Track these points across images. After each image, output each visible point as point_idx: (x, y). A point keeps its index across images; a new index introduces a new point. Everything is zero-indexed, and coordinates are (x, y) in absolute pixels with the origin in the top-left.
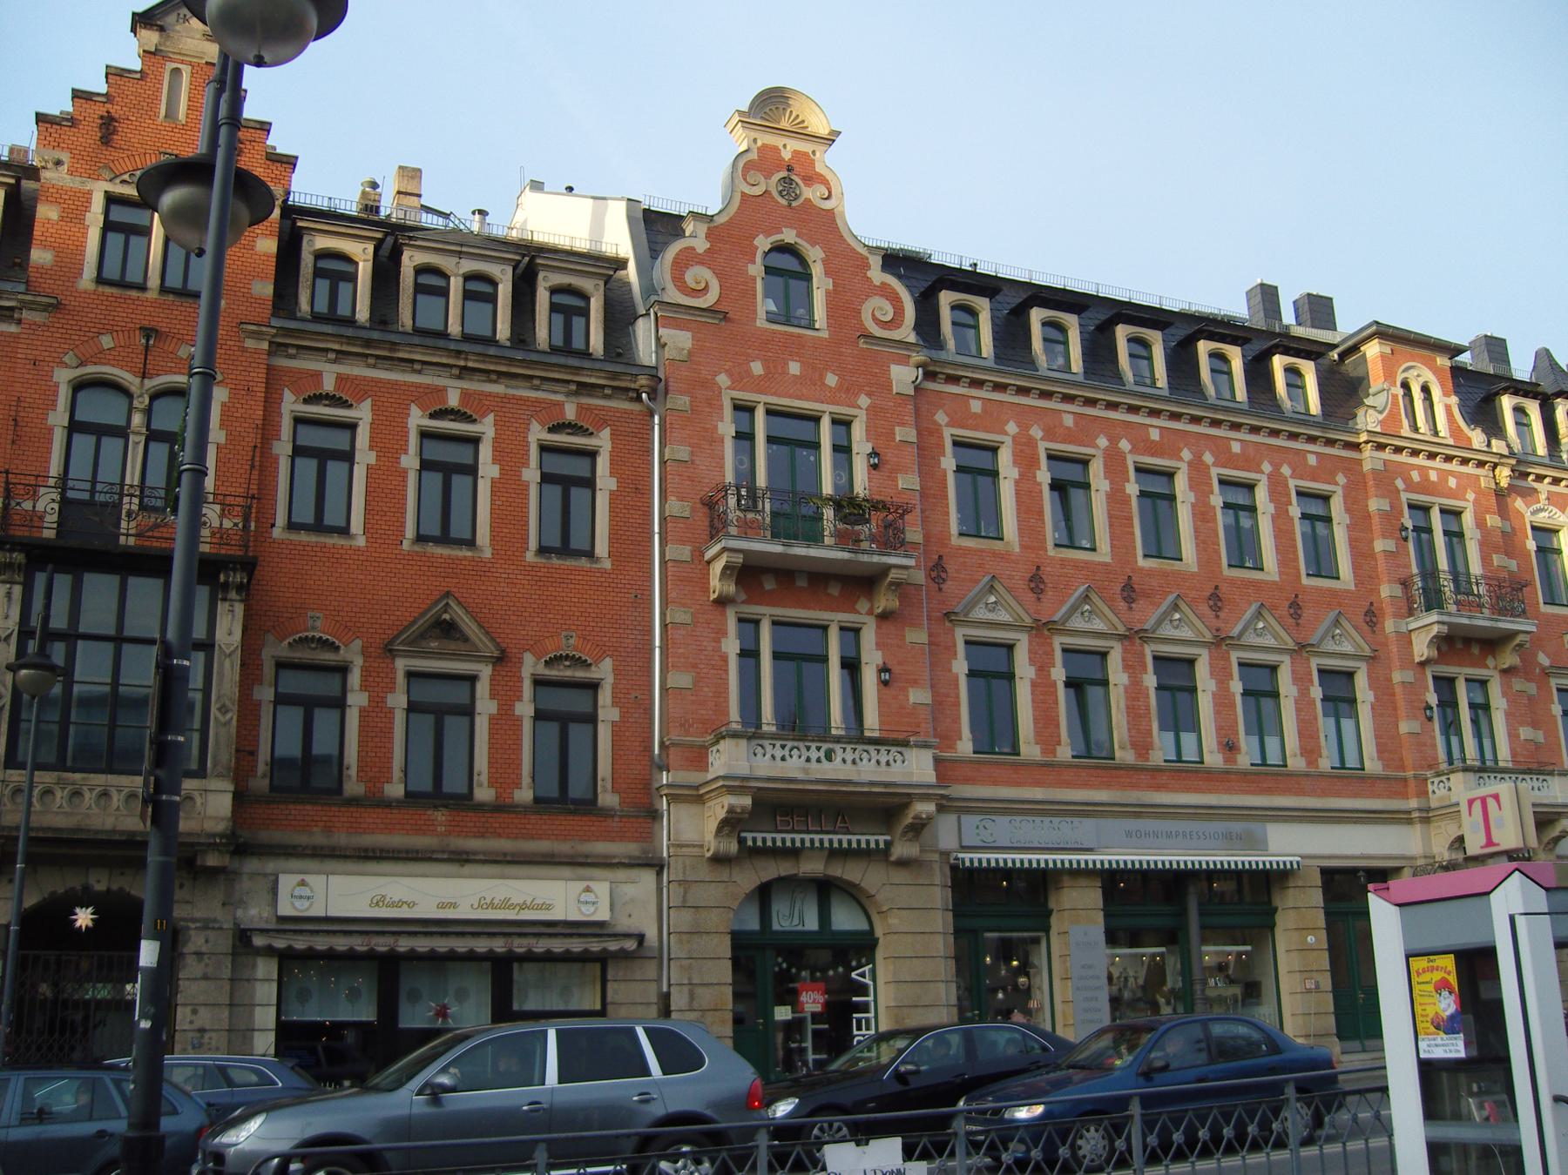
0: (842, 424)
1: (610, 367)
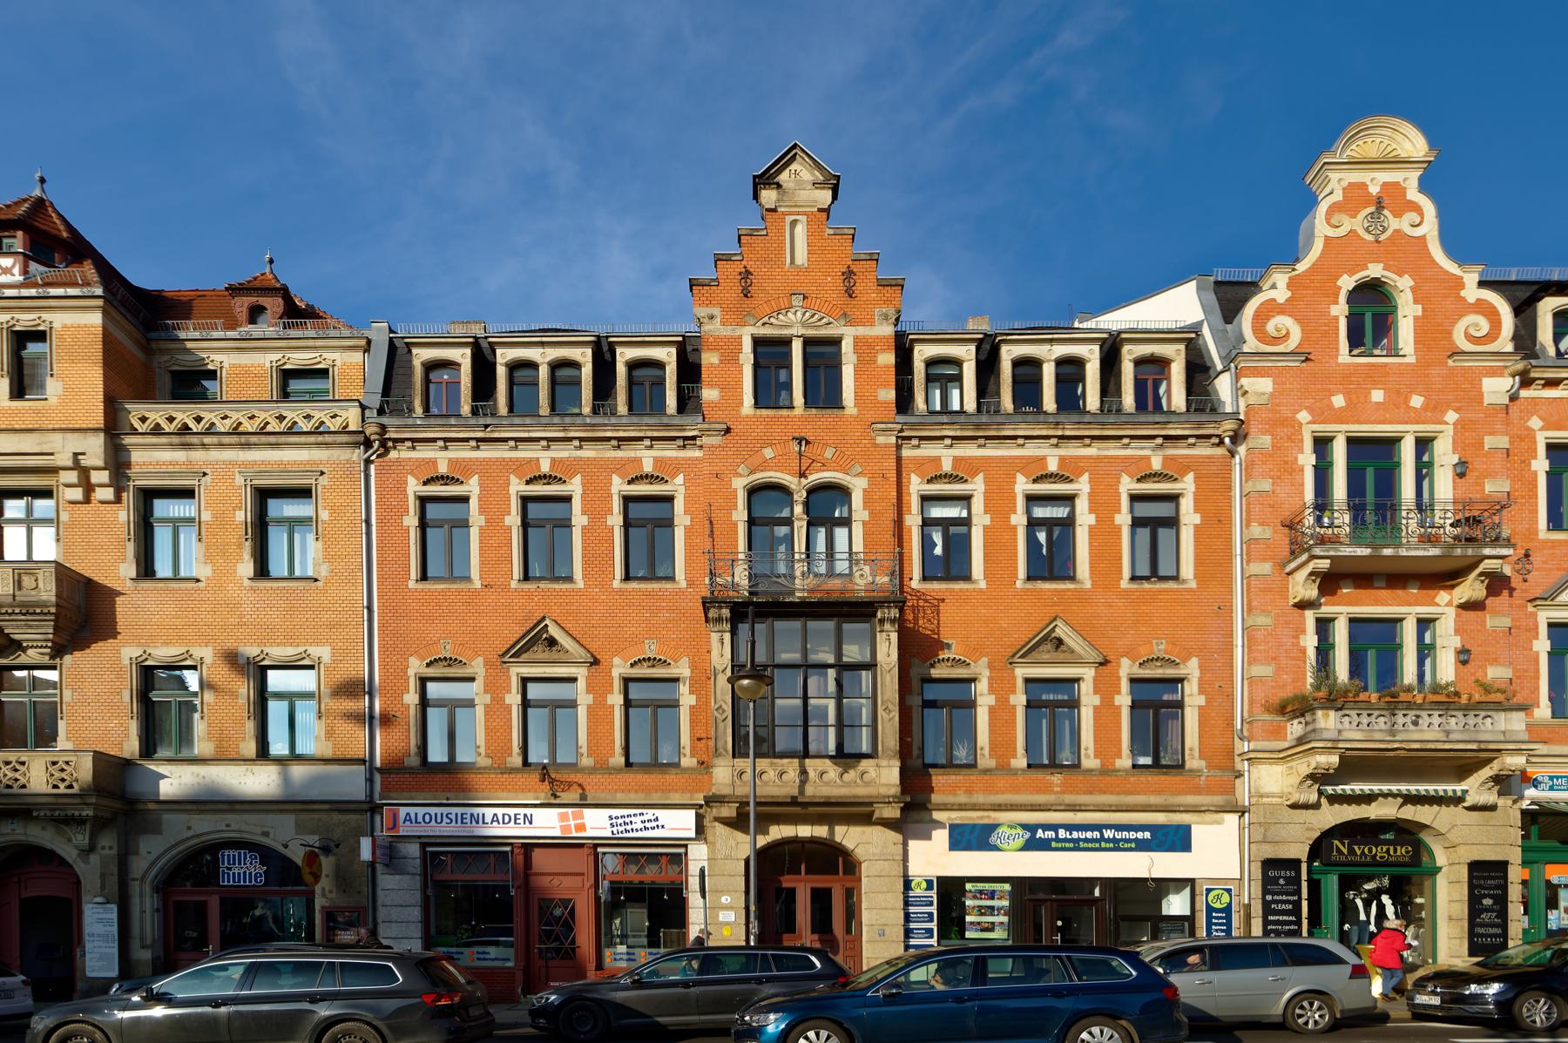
0: (1423, 444)
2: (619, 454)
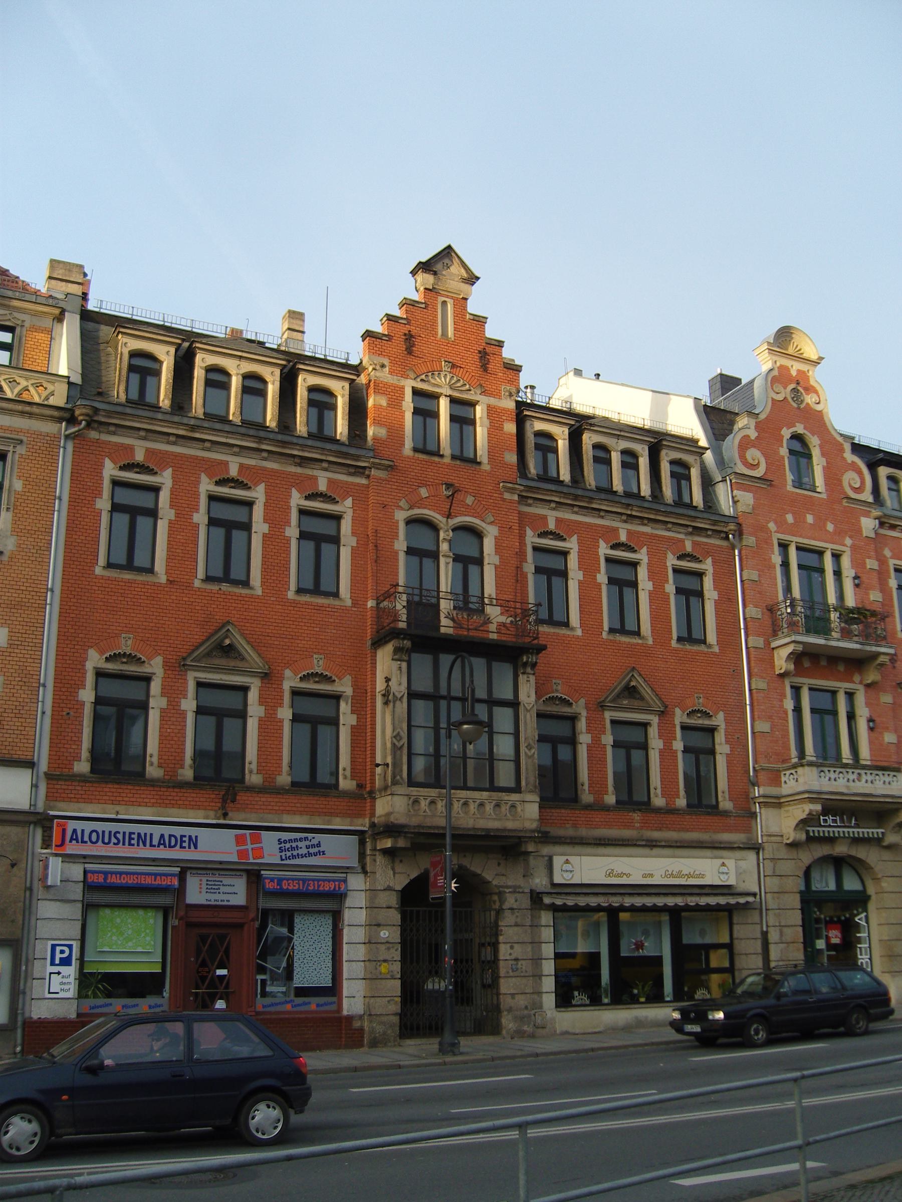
0: (836, 556)
2: (299, 470)
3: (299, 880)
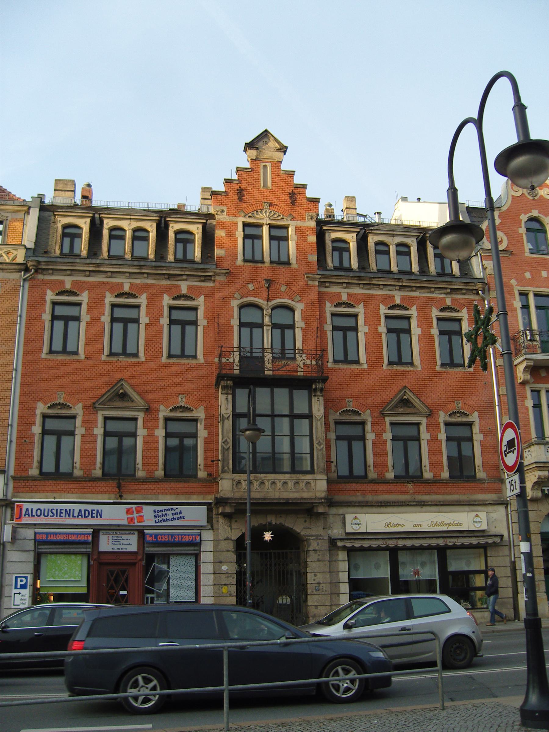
1: (464, 280)
2: (168, 282)
3: (169, 535)
